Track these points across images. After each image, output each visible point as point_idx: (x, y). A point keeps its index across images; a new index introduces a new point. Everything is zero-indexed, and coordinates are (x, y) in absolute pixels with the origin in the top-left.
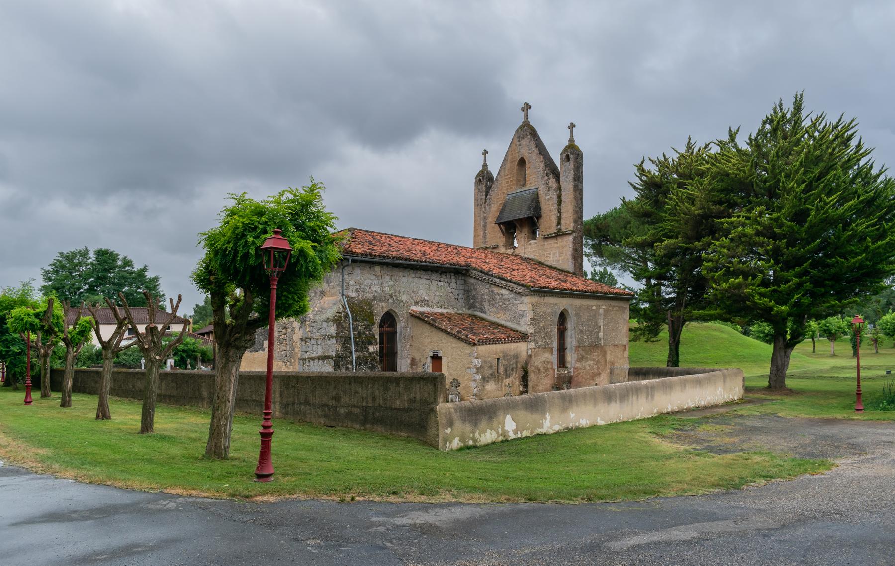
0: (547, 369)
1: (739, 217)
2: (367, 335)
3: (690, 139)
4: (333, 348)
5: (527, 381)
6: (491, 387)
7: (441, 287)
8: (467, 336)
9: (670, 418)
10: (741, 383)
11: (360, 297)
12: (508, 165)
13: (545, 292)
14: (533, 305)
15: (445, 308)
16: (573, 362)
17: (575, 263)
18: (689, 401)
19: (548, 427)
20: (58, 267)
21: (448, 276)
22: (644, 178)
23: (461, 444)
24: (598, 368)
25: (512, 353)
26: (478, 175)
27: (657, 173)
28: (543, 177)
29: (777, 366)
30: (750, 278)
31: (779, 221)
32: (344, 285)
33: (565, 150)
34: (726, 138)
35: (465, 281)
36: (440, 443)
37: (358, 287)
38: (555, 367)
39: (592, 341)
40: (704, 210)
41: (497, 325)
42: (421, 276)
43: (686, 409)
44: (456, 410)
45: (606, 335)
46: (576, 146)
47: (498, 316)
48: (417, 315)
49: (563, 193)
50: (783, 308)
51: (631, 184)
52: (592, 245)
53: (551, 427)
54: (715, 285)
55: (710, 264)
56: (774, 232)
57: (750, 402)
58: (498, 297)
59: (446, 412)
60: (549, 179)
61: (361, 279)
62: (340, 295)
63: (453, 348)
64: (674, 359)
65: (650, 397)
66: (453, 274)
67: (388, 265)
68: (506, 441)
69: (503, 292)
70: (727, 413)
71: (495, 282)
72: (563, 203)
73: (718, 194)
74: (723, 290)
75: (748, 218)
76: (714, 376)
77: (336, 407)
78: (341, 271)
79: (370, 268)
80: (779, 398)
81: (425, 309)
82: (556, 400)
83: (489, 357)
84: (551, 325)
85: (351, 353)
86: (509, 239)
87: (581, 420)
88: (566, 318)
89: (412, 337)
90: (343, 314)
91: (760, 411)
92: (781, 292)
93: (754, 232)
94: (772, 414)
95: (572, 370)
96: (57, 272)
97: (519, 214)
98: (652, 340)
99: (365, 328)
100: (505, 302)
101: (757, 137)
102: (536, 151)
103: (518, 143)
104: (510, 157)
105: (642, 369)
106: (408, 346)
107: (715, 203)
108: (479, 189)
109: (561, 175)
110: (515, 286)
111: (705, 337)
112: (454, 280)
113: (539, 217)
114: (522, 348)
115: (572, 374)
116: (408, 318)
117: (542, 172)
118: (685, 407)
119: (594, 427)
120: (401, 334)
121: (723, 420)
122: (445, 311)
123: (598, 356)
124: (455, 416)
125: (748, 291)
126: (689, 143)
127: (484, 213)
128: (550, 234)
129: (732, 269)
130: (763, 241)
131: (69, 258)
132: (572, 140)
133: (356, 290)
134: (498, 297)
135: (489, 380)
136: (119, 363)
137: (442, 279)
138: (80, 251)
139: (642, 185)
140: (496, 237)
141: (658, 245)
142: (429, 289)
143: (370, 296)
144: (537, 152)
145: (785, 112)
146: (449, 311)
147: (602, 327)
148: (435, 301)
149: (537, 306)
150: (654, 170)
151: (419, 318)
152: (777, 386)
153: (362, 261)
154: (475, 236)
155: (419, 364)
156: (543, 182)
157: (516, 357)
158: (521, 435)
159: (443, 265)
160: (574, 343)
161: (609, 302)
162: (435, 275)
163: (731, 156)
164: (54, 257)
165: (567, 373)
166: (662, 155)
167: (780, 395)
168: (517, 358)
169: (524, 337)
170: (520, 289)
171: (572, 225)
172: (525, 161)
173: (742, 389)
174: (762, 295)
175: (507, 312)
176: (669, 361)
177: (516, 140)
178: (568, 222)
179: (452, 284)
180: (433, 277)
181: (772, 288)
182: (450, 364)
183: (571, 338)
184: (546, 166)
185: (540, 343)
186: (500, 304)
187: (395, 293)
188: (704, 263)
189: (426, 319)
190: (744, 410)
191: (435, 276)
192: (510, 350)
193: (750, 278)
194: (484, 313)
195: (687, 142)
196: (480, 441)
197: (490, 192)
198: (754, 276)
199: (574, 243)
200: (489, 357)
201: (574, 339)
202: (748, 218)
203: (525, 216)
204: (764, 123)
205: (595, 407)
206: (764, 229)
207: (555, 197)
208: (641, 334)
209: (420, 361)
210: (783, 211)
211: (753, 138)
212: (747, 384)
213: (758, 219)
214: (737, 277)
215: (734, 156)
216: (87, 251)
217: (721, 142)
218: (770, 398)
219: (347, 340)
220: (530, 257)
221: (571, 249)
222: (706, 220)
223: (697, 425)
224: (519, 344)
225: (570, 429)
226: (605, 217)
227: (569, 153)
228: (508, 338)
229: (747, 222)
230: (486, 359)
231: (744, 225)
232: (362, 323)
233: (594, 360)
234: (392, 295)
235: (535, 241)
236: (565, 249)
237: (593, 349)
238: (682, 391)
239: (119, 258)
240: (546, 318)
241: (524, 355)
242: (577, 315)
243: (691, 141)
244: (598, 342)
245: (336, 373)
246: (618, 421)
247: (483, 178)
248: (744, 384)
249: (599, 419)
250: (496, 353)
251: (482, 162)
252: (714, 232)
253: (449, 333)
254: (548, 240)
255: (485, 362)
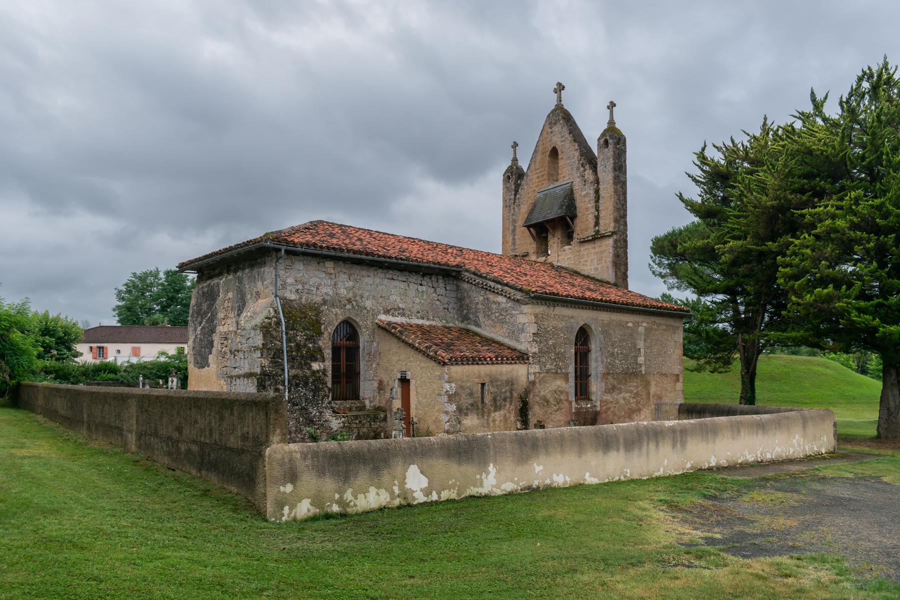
0: (559, 402)
1: (826, 206)
2: (309, 348)
3: (765, 119)
4: (257, 363)
5: (526, 416)
6: (471, 421)
7: (422, 292)
8: (436, 353)
9: (709, 476)
10: (831, 430)
11: (303, 300)
12: (539, 158)
13: (555, 300)
14: (536, 316)
15: (428, 319)
16: (599, 393)
17: (616, 273)
18: (746, 452)
19: (493, 486)
20: (131, 287)
21: (434, 278)
22: (707, 168)
23: (314, 511)
24: (638, 403)
25: (505, 378)
26: (507, 171)
27: (723, 162)
28: (578, 169)
29: (888, 409)
30: (844, 287)
31: (884, 209)
32: (279, 286)
33: (603, 135)
34: (809, 108)
35: (458, 286)
36: (270, 508)
37: (300, 287)
38: (572, 398)
39: (628, 368)
40: (780, 200)
41: (489, 342)
42: (394, 277)
43: (741, 464)
44: (304, 456)
45: (649, 360)
46: (617, 129)
47: (494, 330)
48: (384, 326)
49: (601, 187)
50: (892, 328)
51: (687, 174)
52: (669, 265)
53: (498, 486)
54: (796, 297)
55: (788, 270)
56: (877, 225)
57: (845, 457)
58: (494, 306)
59: (284, 459)
60: (585, 170)
61: (303, 276)
62: (273, 296)
63: (422, 368)
64: (749, 396)
65: (679, 445)
66: (441, 277)
67: (345, 260)
68: (408, 507)
69: (500, 299)
70: (803, 472)
71: (490, 287)
72: (601, 199)
73: (798, 180)
74: (806, 304)
75: (839, 208)
76: (787, 418)
77: (178, 442)
78: (274, 265)
79: (318, 263)
80: (890, 452)
81: (399, 320)
82: (508, 445)
83: (468, 381)
84: (565, 344)
85: (283, 370)
86: (542, 245)
87: (555, 476)
88: (588, 335)
89: (380, 353)
90: (274, 319)
91: (857, 471)
92: (889, 307)
93: (848, 225)
94: (873, 478)
95: (598, 404)
96: (129, 292)
97: (550, 213)
98: (720, 370)
99: (306, 340)
100: (502, 313)
101: (850, 98)
102: (570, 138)
103: (550, 130)
104: (541, 148)
105: (696, 405)
106: (374, 366)
107: (794, 191)
108: (507, 188)
109: (599, 165)
110: (512, 291)
111: (804, 372)
112: (442, 285)
113: (573, 217)
114: (521, 372)
115: (598, 409)
116: (374, 329)
117: (577, 162)
118: (740, 461)
119: (578, 488)
120: (364, 349)
121: (792, 483)
122: (426, 323)
123: (637, 387)
124: (301, 465)
125: (841, 304)
126: (765, 124)
127: (513, 215)
128: (587, 237)
129: (818, 275)
130: (861, 238)
131: (143, 278)
132: (611, 122)
133: (297, 290)
134: (494, 306)
135: (469, 412)
136: (117, 380)
137: (424, 283)
138: (152, 272)
139: (704, 178)
140: (526, 243)
141: (720, 248)
142: (405, 295)
143: (318, 299)
144: (570, 139)
145: (891, 72)
146: (434, 323)
147: (642, 351)
148: (415, 310)
149: (543, 318)
150: (718, 157)
151: (386, 329)
152: (890, 436)
153: (305, 254)
154: (503, 243)
155: (387, 389)
156: (578, 175)
157: (511, 383)
158: (439, 497)
159: (421, 264)
160: (601, 369)
161: (653, 319)
162: (415, 277)
163: (816, 130)
164: (126, 277)
165: (591, 408)
166: (730, 140)
167: (893, 448)
168: (512, 384)
169: (522, 357)
170: (519, 295)
171: (612, 225)
172: (557, 150)
173: (833, 438)
174: (860, 310)
175: (504, 326)
176: (741, 397)
177: (548, 126)
178: (607, 222)
179: (438, 290)
180: (411, 280)
181: (876, 301)
182: (419, 390)
183: (597, 362)
184: (581, 155)
185: (548, 366)
186: (497, 315)
187: (355, 297)
188: (780, 269)
189: (393, 331)
190: (829, 470)
191: (414, 278)
192: (501, 374)
193: (844, 287)
194: (478, 325)
195: (762, 124)
196: (355, 505)
197: (520, 191)
198: (850, 285)
199: (616, 247)
200: (468, 381)
201: (600, 363)
202: (839, 208)
203: (557, 216)
204: (860, 79)
205: (580, 457)
206: (862, 221)
207: (592, 192)
208: (706, 363)
209: (388, 385)
210: (889, 195)
211: (844, 100)
212: (842, 431)
213: (854, 207)
214: (826, 287)
215: (820, 130)
216: (158, 272)
217: (802, 114)
218: (876, 452)
219: (278, 353)
220: (563, 265)
221: (611, 255)
222: (784, 214)
223: (745, 491)
224: (515, 366)
225: (534, 490)
226: (681, 232)
227: (608, 138)
228: (497, 357)
229: (838, 212)
230: (463, 384)
231: (833, 217)
232: (302, 332)
233: (631, 392)
234: (350, 299)
235: (570, 247)
236: (604, 254)
237: (630, 378)
238: (733, 438)
239: (188, 279)
240: (558, 334)
241: (523, 381)
242: (605, 333)
243: (767, 122)
244: (636, 369)
245: (260, 395)
246: (622, 478)
247: (512, 175)
248: (835, 431)
249: (588, 474)
250: (479, 376)
251: (608, 119)
252: (794, 228)
253: (417, 349)
254: (584, 244)
255: (462, 387)
